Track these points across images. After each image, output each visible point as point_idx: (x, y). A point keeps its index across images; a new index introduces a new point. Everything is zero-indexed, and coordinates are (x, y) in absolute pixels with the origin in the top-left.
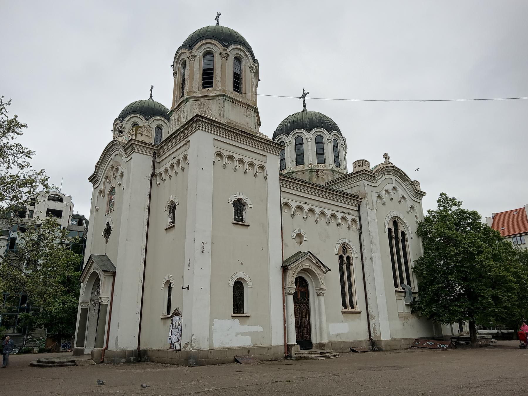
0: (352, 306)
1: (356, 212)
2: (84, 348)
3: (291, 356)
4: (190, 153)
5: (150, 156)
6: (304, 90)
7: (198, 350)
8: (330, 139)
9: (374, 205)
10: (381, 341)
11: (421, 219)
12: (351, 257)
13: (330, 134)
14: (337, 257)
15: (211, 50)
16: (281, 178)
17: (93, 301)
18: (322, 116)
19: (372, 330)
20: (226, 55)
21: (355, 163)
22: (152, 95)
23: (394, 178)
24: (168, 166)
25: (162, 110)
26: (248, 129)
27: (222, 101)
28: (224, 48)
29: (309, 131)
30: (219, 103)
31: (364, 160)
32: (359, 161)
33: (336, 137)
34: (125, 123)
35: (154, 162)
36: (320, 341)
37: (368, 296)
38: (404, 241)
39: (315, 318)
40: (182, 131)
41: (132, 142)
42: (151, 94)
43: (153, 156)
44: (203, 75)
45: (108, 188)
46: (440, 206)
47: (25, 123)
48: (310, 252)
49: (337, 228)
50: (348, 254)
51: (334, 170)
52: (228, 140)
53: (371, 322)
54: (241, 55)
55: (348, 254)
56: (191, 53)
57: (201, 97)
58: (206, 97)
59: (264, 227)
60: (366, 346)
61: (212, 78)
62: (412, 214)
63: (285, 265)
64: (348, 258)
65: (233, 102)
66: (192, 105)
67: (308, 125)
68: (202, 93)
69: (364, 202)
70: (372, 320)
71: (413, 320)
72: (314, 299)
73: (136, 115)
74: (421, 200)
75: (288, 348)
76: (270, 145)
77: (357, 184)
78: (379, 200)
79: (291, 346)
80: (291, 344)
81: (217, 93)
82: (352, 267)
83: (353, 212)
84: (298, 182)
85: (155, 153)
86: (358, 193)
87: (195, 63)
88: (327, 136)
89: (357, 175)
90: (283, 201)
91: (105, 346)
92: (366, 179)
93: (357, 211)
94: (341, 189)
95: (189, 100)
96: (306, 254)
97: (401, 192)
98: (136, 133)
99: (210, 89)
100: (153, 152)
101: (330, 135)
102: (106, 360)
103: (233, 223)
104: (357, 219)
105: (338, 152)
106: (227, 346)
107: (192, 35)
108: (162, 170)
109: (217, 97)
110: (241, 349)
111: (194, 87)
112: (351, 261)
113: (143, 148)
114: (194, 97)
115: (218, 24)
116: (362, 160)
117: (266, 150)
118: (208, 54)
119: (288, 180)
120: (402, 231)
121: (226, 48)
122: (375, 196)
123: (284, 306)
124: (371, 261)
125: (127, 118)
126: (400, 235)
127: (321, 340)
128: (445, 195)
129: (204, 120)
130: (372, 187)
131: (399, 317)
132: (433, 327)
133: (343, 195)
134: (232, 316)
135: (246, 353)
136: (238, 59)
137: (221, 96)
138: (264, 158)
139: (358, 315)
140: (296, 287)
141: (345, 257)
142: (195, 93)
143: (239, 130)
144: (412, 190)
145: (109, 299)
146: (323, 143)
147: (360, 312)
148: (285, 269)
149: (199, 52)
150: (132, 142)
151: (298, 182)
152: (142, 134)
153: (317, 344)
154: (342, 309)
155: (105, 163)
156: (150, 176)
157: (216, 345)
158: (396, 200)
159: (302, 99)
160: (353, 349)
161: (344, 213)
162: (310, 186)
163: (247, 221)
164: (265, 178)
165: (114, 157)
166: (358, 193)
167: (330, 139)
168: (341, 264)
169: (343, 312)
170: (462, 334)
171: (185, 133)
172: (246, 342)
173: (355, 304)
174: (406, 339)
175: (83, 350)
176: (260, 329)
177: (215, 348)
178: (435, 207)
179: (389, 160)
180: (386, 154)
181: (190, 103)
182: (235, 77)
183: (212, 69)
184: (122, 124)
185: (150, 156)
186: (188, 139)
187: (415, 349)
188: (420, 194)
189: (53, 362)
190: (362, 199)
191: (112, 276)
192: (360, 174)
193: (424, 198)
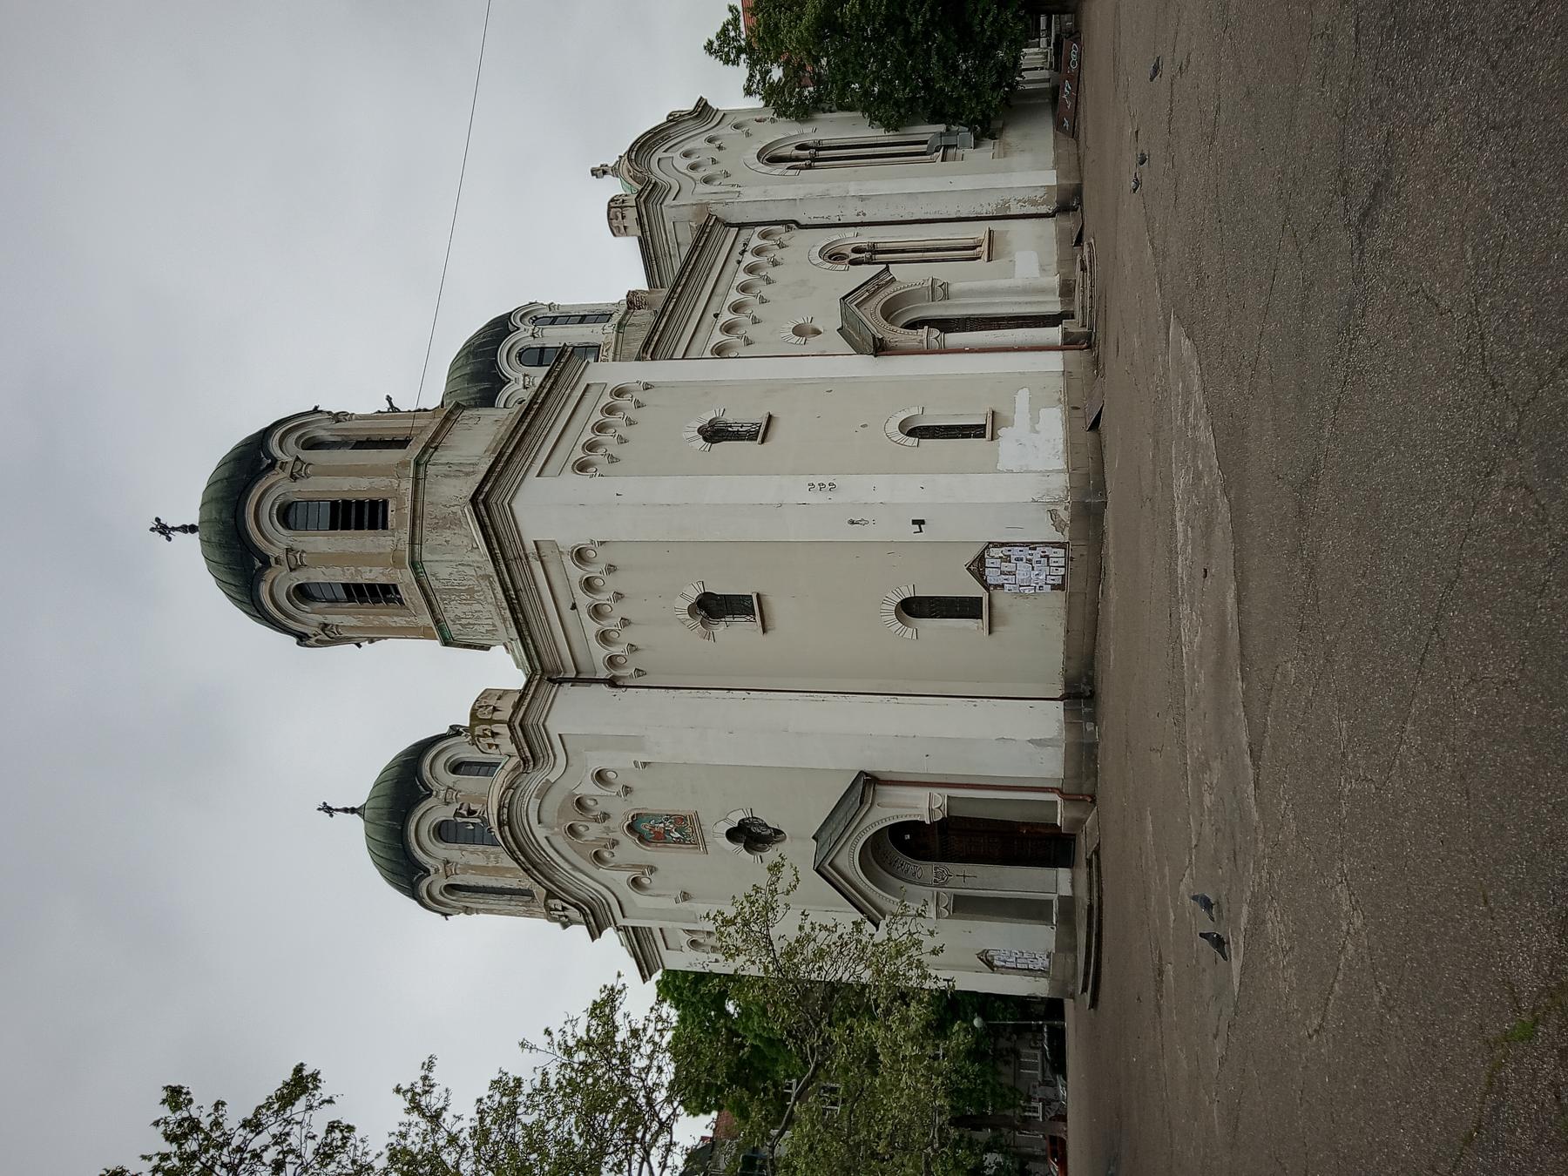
1: (741, 232)
2: (1054, 897)
3: (1088, 337)
4: (569, 540)
5: (557, 690)
7: (1068, 491)
8: (533, 330)
9: (727, 190)
11: (770, 113)
13: (518, 329)
15: (276, 507)
16: (649, 356)
17: (935, 881)
18: (466, 351)
19: (1033, 210)
21: (614, 229)
22: (349, 807)
23: (659, 154)
24: (592, 627)
25: (404, 761)
26: (508, 422)
27: (431, 470)
28: (277, 468)
29: (502, 382)
30: (437, 476)
31: (609, 205)
32: (611, 216)
33: (526, 320)
34: (431, 861)
35: (576, 681)
36: (1055, 294)
37: (954, 216)
39: (1002, 304)
40: (506, 566)
41: (517, 724)
42: (346, 810)
43: (560, 683)
44: (349, 528)
45: (629, 849)
46: (735, 62)
47: (420, 1068)
48: (844, 298)
49: (781, 266)
50: (848, 251)
51: (620, 324)
52: (544, 446)
53: (1014, 211)
54: (300, 437)
56: (277, 561)
57: (413, 525)
58: (414, 510)
59: (772, 388)
60: (1069, 222)
61: (360, 504)
62: (753, 127)
64: (856, 250)
65: (436, 448)
66: (433, 551)
67: (486, 385)
68: (400, 525)
70: (1009, 207)
71: (1012, 136)
72: (957, 305)
73: (412, 827)
74: (718, 110)
75: (1069, 342)
76: (559, 375)
77: (669, 226)
79: (1066, 335)
80: (1060, 335)
81: (407, 485)
83: (741, 240)
84: (662, 325)
85: (550, 680)
86: (695, 226)
87: (309, 548)
88: (523, 336)
89: (646, 222)
91: (1054, 797)
92: (660, 202)
93: (739, 230)
94: (677, 266)
95: (417, 559)
97: (698, 143)
98: (491, 722)
99: (391, 507)
100: (546, 686)
101: (522, 329)
102: (1086, 788)
103: (763, 442)
105: (570, 316)
106: (1061, 447)
108: (600, 653)
109: (418, 483)
110: (1069, 423)
111: (382, 550)
113: (536, 704)
114: (412, 543)
115: (187, 529)
116: (610, 208)
117: (572, 384)
118: (286, 514)
119: (654, 343)
121: (279, 463)
122: (703, 188)
123: (972, 351)
124: (869, 199)
125: (419, 854)
127: (1052, 291)
128: (711, 43)
129: (486, 489)
130: (680, 194)
131: (1004, 157)
132: (1031, 102)
133: (699, 249)
134: (992, 439)
135: (1079, 413)
136: (457, 767)
137: (417, 472)
138: (593, 390)
140: (926, 327)
142: (399, 545)
143: (516, 427)
144: (691, 122)
145: (935, 791)
146: (542, 349)
147: (990, 231)
148: (880, 348)
149: (433, 853)
150: (517, 724)
151: (662, 325)
152: (494, 707)
153: (1061, 301)
155: (553, 866)
156: (615, 690)
157: (1060, 464)
158: (716, 155)
161: (744, 251)
162: (672, 304)
164: (647, 387)
165: (545, 827)
166: (695, 226)
167: (533, 330)
171: (512, 557)
172: (1053, 423)
173: (970, 243)
174: (1056, 147)
175: (1061, 898)
176: (1023, 397)
177: (1066, 467)
178: (740, 73)
179: (611, 165)
180: (594, 172)
181: (426, 556)
183: (334, 504)
184: (432, 870)
185: (557, 690)
186: (531, 548)
187: (1079, 124)
188: (702, 110)
189: (1090, 907)
190: (710, 216)
191: (878, 787)
192: (644, 213)
193: (713, 104)
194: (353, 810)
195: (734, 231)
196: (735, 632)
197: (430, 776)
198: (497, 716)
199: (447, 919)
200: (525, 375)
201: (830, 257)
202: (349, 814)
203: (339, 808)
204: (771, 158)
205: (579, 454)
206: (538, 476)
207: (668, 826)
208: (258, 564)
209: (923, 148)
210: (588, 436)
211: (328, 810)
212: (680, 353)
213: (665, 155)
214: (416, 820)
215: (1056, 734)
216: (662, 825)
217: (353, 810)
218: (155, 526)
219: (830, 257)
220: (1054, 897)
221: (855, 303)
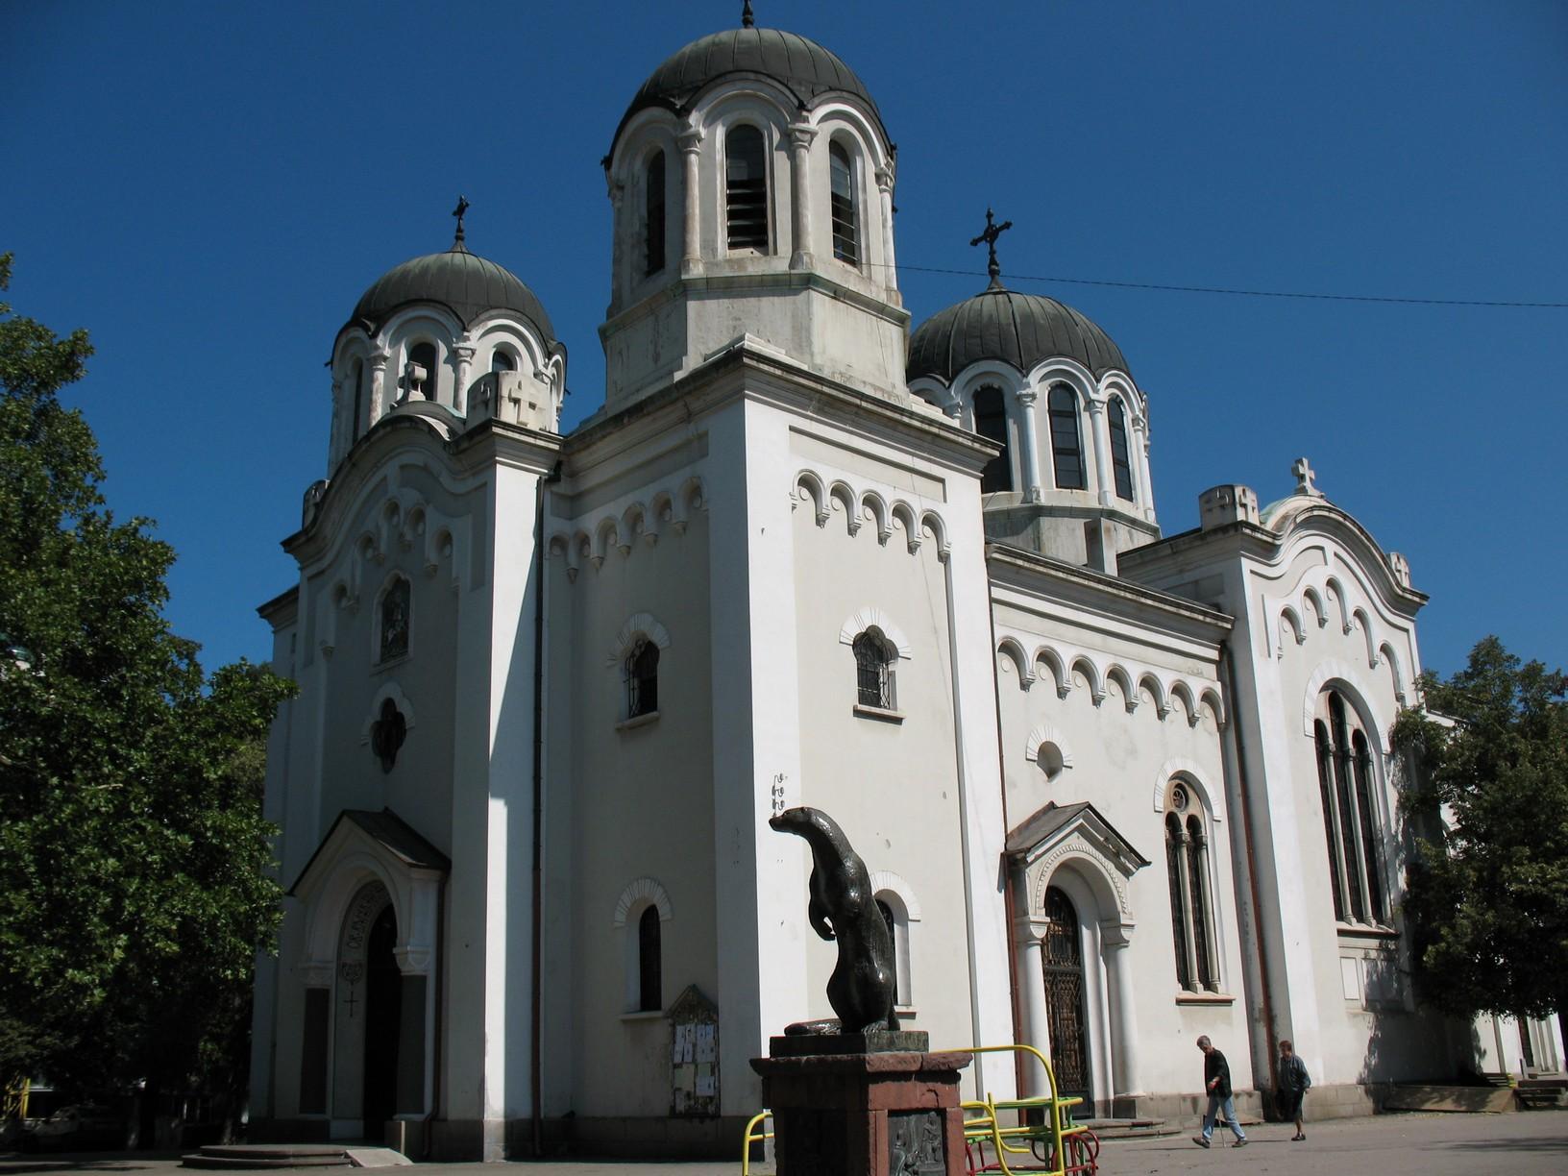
0: (1209, 986)
6: (989, 216)
12: (1199, 817)
14: (1161, 820)
23: (1331, 547)
48: (1090, 807)
64: (1194, 823)
81: (780, 264)
90: (1000, 634)
120: (1356, 727)
140: (1048, 920)
141: (1183, 820)
154: (1177, 990)
159: (984, 246)
163: (903, 708)
168: (1174, 844)
169: (1179, 1002)
182: (836, 212)
196: (613, 690)
199: (326, 365)
204: (1338, 694)
205: (827, 478)
206: (792, 429)
208: (679, 104)
211: (460, 211)
212: (997, 593)
214: (437, 317)
216: (400, 617)
219: (1179, 786)
220: (328, 1116)
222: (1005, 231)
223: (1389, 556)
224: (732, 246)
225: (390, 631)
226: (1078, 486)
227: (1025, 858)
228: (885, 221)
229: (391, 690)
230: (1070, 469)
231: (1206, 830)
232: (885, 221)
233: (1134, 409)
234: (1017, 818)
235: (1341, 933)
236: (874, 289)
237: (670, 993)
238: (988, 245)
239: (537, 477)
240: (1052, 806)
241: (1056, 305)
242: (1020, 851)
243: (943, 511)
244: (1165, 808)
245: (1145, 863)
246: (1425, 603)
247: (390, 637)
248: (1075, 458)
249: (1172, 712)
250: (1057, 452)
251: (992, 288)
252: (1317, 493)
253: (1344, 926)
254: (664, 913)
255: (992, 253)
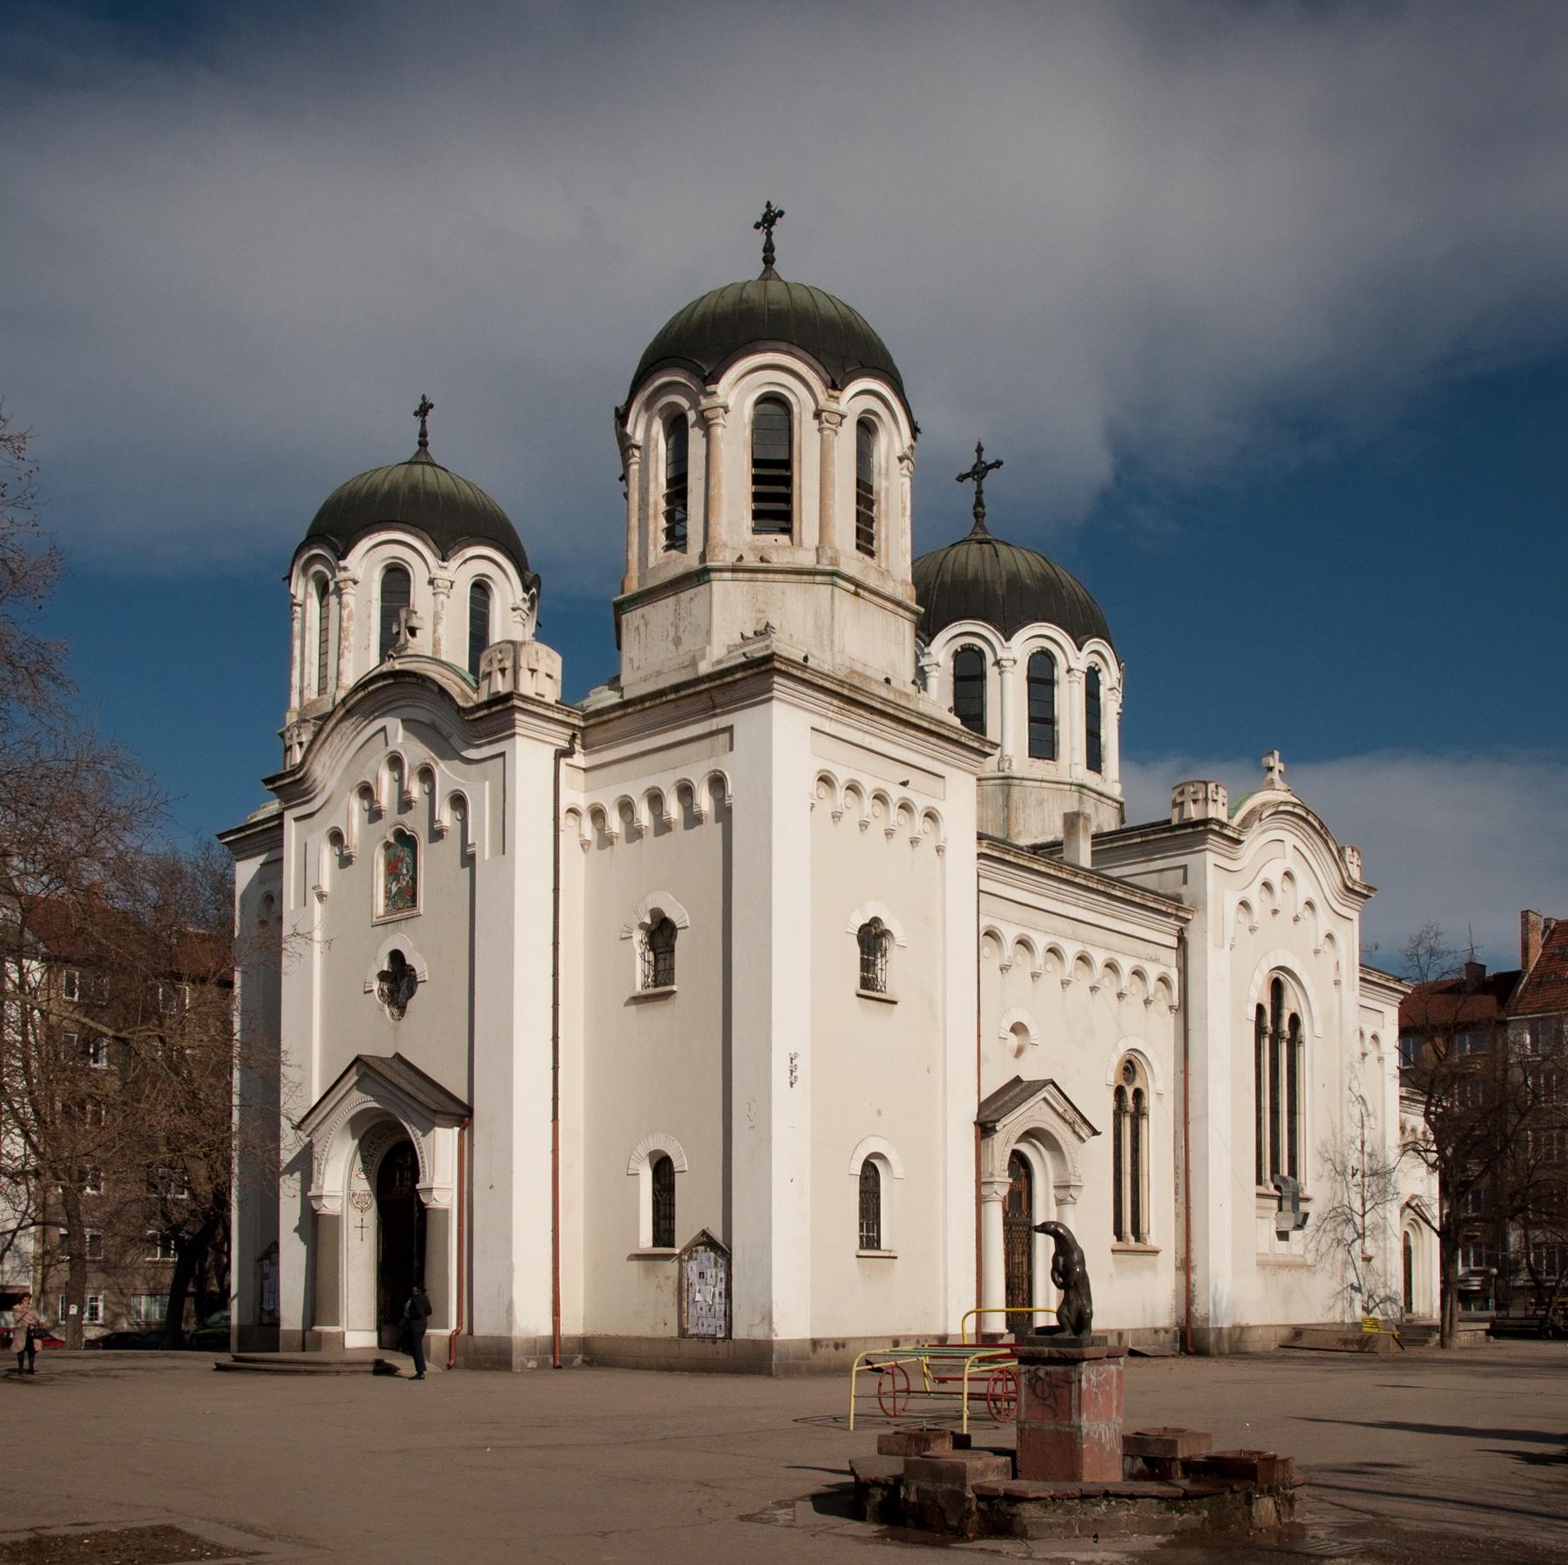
6: (979, 450)
10: (1207, 1330)
20: (838, 419)
23: (1291, 840)
38: (1295, 1041)
42: (423, 434)
49: (831, 823)
50: (1138, 1084)
55: (1138, 1084)
63: (983, 1119)
64: (1138, 1094)
69: (1195, 919)
78: (1241, 917)
81: (807, 559)
82: (1144, 1123)
85: (574, 736)
90: (986, 922)
91: (453, 1325)
96: (1042, 1084)
103: (859, 996)
104: (1174, 976)
107: (693, 306)
112: (1145, 1103)
120: (1293, 1011)
126: (1285, 1025)
135: (809, 1347)
139: (1150, 1258)
140: (1011, 1180)
141: (1129, 1091)
148: (985, 1129)
159: (971, 484)
160: (1136, 1348)
170: (1409, 1316)
173: (1144, 1228)
194: (423, 444)
195: (1173, 942)
197: (467, 556)
198: (525, 675)
200: (1015, 661)
201: (1130, 1062)
202: (418, 439)
203: (427, 424)
205: (842, 776)
207: (404, 880)
209: (1284, 1171)
210: (869, 785)
213: (1290, 849)
215: (522, 1327)
217: (423, 444)
218: (773, 209)
221: (1049, 1098)
222: (995, 470)
223: (1343, 848)
224: (755, 531)
225: (394, 883)
226: (1050, 756)
227: (995, 1127)
228: (904, 509)
229: (399, 940)
230: (1043, 742)
231: (1151, 1102)
232: (904, 509)
233: (1110, 677)
234: (987, 1092)
235: (1259, 1195)
236: (891, 583)
237: (684, 1233)
238: (975, 482)
239: (554, 748)
240: (1017, 1080)
241: (1041, 559)
242: (991, 1122)
243: (942, 808)
244: (1115, 1082)
245: (1095, 1133)
246: (1372, 895)
247: (394, 889)
248: (1050, 726)
249: (1129, 995)
250: (1032, 719)
251: (976, 534)
252: (1283, 786)
253: (1262, 1190)
254: (679, 1163)
255: (979, 492)
